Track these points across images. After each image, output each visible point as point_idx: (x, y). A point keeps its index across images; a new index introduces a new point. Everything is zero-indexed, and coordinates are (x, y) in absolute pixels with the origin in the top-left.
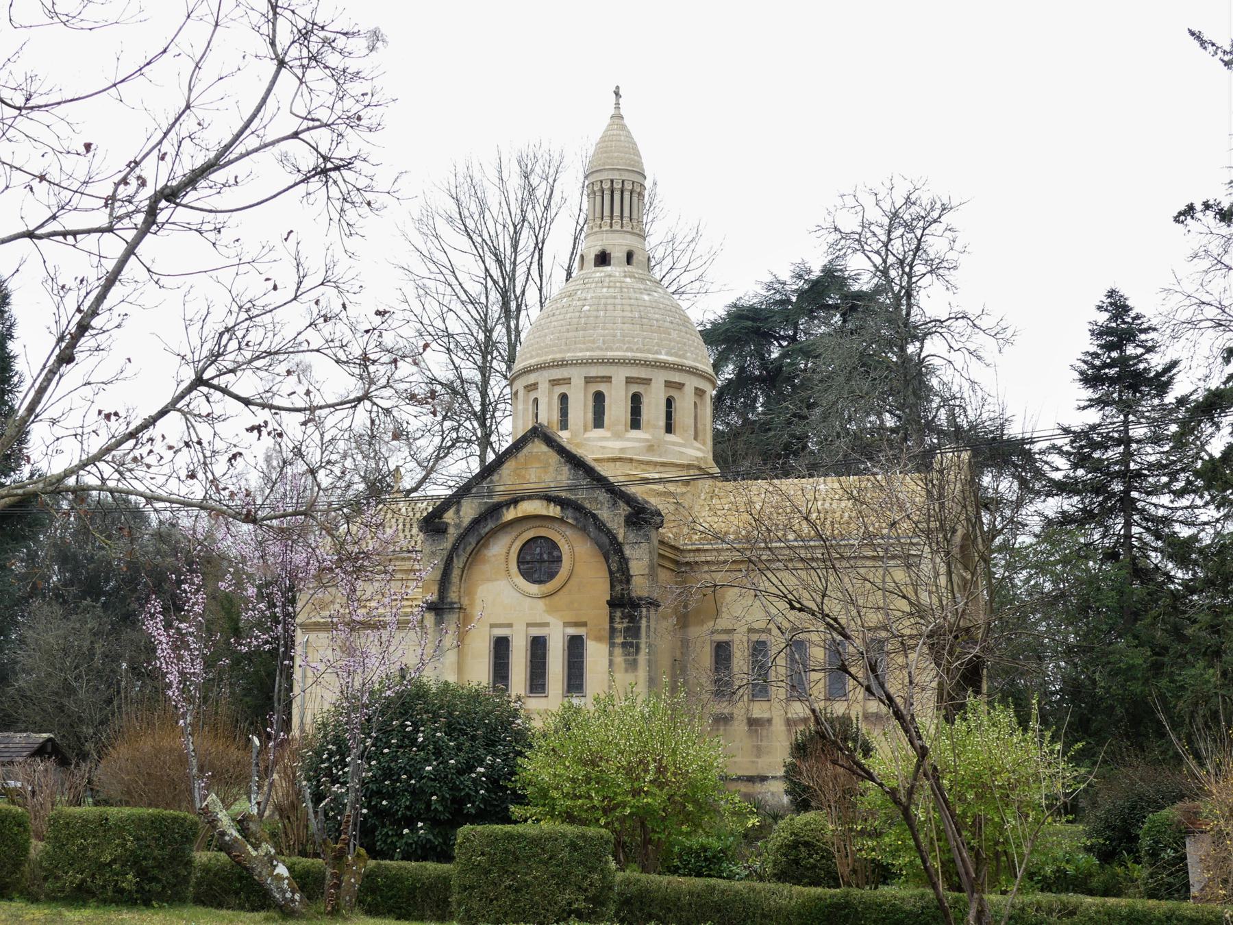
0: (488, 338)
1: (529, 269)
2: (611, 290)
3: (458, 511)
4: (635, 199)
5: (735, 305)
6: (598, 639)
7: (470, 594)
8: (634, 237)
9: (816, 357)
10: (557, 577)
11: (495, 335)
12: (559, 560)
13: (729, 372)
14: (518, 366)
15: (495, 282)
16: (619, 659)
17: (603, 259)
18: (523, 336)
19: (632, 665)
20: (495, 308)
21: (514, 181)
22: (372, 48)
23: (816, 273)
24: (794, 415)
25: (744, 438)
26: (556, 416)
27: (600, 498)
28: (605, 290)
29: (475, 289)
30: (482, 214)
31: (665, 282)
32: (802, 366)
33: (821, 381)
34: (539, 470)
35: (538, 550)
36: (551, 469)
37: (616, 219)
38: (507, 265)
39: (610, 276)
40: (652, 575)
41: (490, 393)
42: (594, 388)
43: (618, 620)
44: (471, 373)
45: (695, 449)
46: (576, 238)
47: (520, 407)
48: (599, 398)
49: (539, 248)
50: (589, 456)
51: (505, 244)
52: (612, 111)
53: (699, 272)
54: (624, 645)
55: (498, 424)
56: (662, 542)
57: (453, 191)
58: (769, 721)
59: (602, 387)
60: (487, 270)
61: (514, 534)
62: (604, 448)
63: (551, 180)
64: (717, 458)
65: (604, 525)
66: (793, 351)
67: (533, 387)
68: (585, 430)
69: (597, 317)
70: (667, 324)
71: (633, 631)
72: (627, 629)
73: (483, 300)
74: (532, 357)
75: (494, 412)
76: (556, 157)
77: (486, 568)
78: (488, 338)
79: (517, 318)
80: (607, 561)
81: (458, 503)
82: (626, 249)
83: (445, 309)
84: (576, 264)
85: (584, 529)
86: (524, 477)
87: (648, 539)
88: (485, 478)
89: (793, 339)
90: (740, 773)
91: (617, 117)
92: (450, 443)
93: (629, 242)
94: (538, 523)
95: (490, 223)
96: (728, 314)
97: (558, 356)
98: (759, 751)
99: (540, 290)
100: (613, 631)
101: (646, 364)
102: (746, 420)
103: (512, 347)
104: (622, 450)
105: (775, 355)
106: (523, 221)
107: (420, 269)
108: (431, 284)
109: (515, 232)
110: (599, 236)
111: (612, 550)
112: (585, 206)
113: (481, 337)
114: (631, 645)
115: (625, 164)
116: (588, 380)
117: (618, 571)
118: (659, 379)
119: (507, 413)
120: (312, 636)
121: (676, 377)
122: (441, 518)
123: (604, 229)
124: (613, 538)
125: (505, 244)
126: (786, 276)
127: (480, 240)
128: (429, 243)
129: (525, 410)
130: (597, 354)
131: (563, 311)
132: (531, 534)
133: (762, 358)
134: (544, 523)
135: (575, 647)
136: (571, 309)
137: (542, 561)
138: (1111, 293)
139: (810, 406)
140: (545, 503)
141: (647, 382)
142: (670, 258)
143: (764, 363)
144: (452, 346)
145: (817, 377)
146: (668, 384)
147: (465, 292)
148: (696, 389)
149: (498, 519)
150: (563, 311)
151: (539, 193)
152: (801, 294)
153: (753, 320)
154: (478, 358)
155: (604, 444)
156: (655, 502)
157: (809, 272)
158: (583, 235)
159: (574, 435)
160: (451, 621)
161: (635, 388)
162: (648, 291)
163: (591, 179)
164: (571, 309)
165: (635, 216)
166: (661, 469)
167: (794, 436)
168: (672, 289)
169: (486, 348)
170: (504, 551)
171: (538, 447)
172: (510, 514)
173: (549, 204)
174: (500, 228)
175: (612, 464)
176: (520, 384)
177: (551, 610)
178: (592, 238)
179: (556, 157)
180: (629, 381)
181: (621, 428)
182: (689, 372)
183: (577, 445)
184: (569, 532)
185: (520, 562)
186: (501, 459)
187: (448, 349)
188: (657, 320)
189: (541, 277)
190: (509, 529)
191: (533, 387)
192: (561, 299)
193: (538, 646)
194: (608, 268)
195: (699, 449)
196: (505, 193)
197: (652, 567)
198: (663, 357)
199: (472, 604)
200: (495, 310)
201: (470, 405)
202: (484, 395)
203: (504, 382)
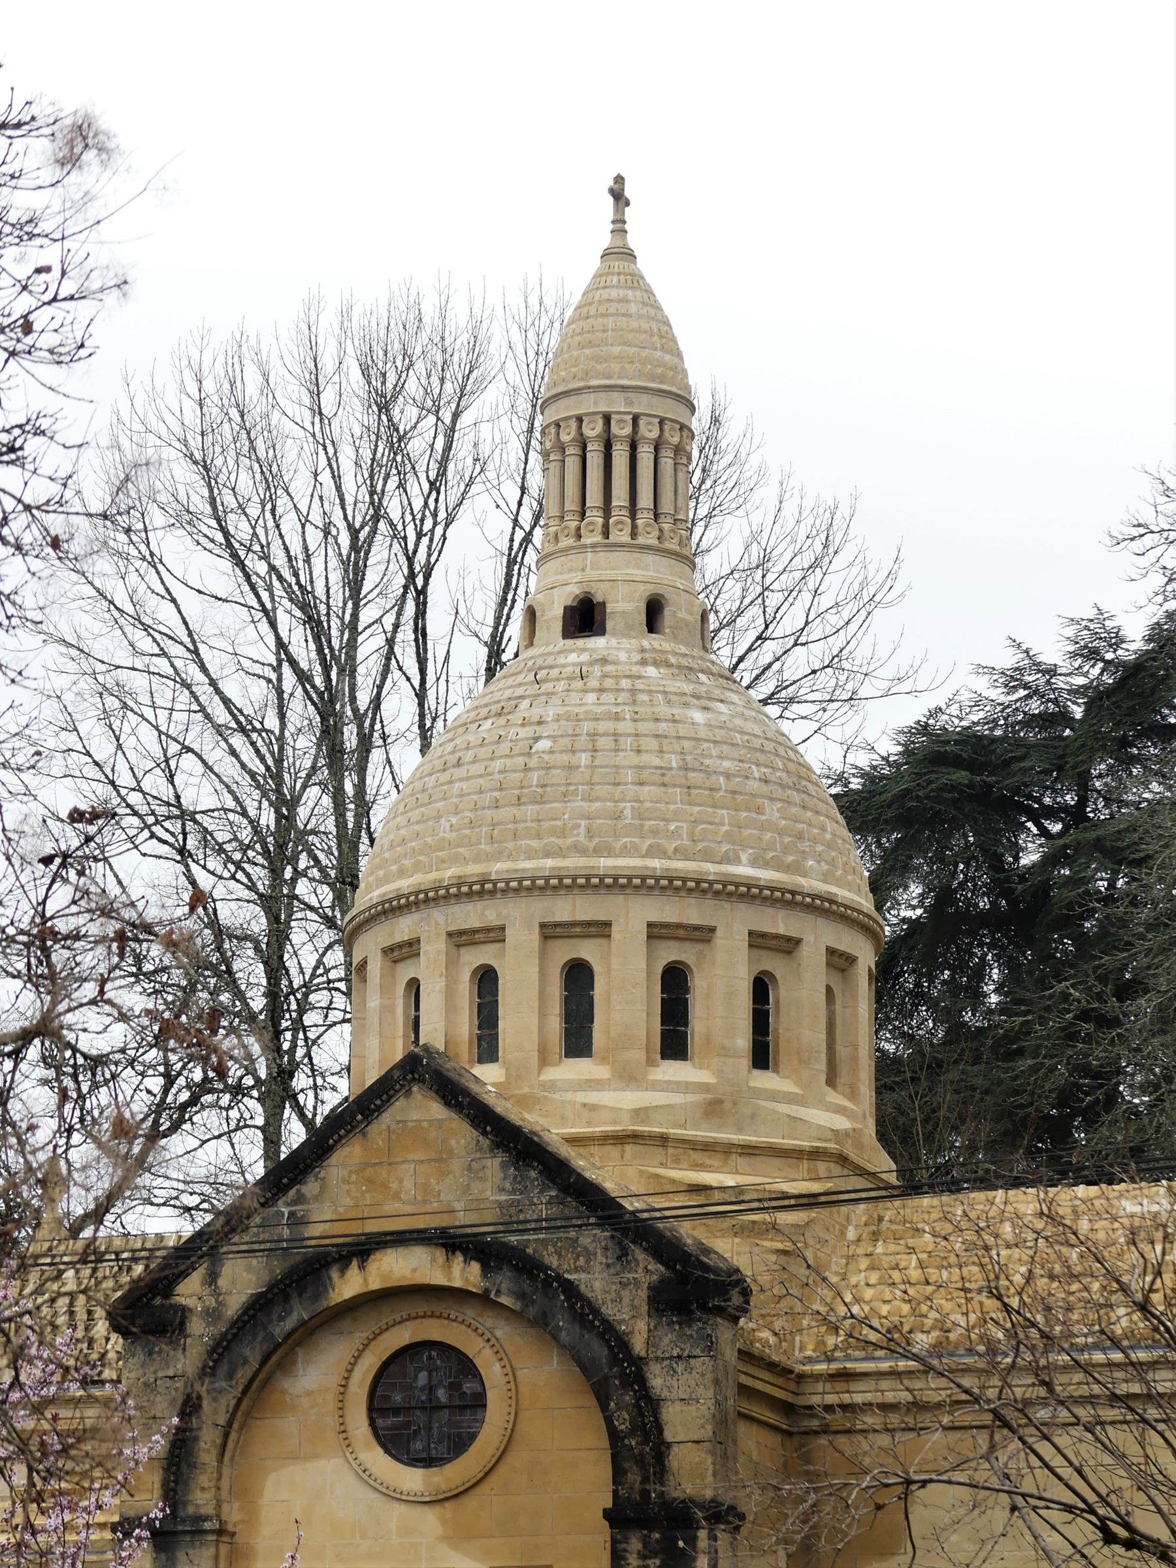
0: (286, 820)
1: (390, 642)
2: (608, 698)
3: (212, 1278)
4: (667, 463)
5: (924, 729)
7: (247, 1493)
8: (666, 561)
9: (1138, 863)
10: (474, 1449)
11: (302, 812)
12: (478, 1402)
13: (910, 903)
14: (367, 896)
15: (303, 677)
17: (585, 618)
18: (377, 816)
20: (303, 742)
21: (352, 419)
22: (69, 161)
23: (1135, 636)
24: (1084, 1016)
25: (953, 1075)
26: (466, 1025)
28: (591, 698)
29: (250, 694)
30: (269, 503)
31: (745, 675)
32: (1102, 885)
33: (1150, 927)
34: (429, 1175)
36: (456, 1165)
37: (619, 514)
38: (335, 633)
39: (604, 661)
40: (722, 1444)
41: (291, 964)
42: (565, 952)
44: (239, 911)
45: (827, 1110)
46: (511, 562)
47: (374, 1002)
48: (578, 977)
49: (416, 587)
50: (553, 1127)
51: (325, 575)
52: (605, 240)
53: (836, 643)
55: (310, 1044)
56: (746, 1355)
57: (195, 442)
59: (587, 950)
60: (281, 645)
61: (359, 1337)
62: (593, 1108)
63: (447, 416)
64: (891, 1131)
65: (596, 1312)
66: (1078, 846)
67: (406, 951)
68: (544, 1061)
69: (570, 768)
70: (753, 785)
73: (272, 722)
74: (402, 873)
75: (301, 1011)
76: (460, 357)
78: (286, 820)
79: (362, 771)
80: (604, 1407)
82: (643, 592)
83: (174, 748)
84: (515, 629)
85: (542, 1323)
86: (385, 1186)
87: (710, 1347)
88: (284, 1190)
89: (1076, 816)
91: (619, 253)
92: (185, 1096)
93: (653, 573)
94: (422, 1307)
95: (289, 524)
96: (907, 752)
97: (473, 870)
99: (421, 695)
101: (700, 888)
102: (957, 1030)
103: (348, 844)
104: (639, 1113)
105: (1030, 858)
106: (376, 518)
107: (109, 645)
108: (138, 683)
109: (354, 546)
110: (575, 559)
111: (616, 1381)
112: (535, 480)
113: (268, 818)
115: (640, 374)
116: (550, 932)
117: (632, 1432)
118: (734, 926)
119: (335, 1016)
121: (780, 923)
122: (168, 1292)
123: (587, 540)
124: (618, 1344)
125: (325, 575)
126: (1053, 652)
127: (262, 568)
128: (133, 578)
129: (387, 1010)
130: (573, 863)
131: (484, 752)
132: (402, 1336)
133: (996, 864)
134: (438, 1308)
136: (504, 748)
137: (432, 1407)
139: (1127, 991)
140: (440, 1254)
141: (702, 934)
142: (756, 610)
143: (1003, 878)
144: (191, 843)
145: (1145, 914)
146: (758, 940)
147: (227, 702)
148: (831, 952)
149: (317, 1297)
150: (484, 752)
151: (416, 446)
152: (1096, 698)
153: (972, 766)
154: (260, 874)
155: (593, 1097)
156: (729, 1249)
157: (1117, 641)
158: (531, 557)
159: (515, 1075)
161: (671, 953)
162: (704, 701)
163: (556, 412)
164: (504, 748)
165: (666, 506)
166: (742, 1162)
167: (1086, 1071)
168: (765, 688)
169: (281, 846)
170: (334, 1380)
171: (421, 1109)
172: (348, 1285)
173: (442, 471)
174: (314, 537)
175: (614, 1151)
176: (370, 946)
178: (553, 564)
179: (460, 357)
180: (657, 932)
181: (639, 1055)
182: (811, 908)
183: (525, 1102)
184: (503, 1331)
185: (376, 1408)
186: (326, 1138)
187: (182, 851)
188: (727, 775)
189: (423, 671)
190: (346, 1324)
191: (406, 951)
192: (478, 721)
194: (597, 643)
195: (840, 1110)
196: (326, 445)
197: (723, 1423)
198: (743, 870)
199: (251, 1520)
200: (304, 747)
201: (239, 995)
202: (275, 969)
203: (328, 936)
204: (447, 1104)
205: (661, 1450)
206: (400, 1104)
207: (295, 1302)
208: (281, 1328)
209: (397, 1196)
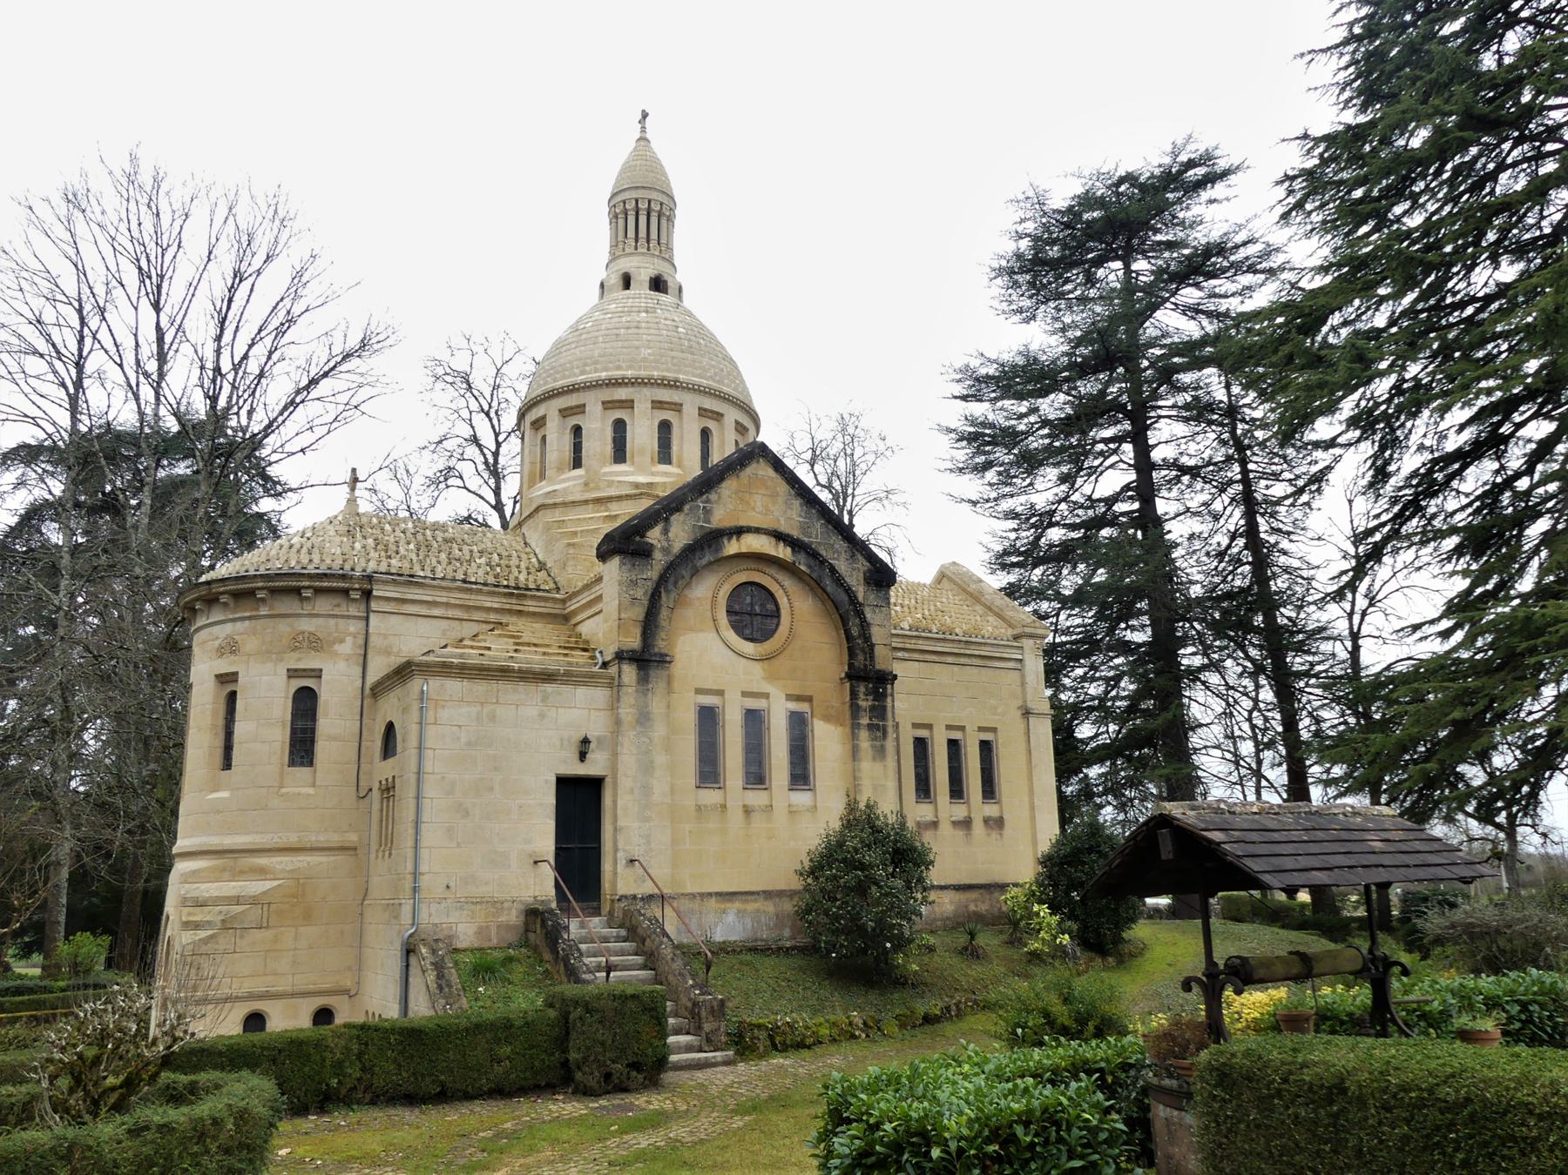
3: (666, 531)
4: (664, 222)
6: (827, 718)
35: (748, 600)
36: (780, 500)
37: (642, 241)
43: (862, 696)
52: (638, 135)
54: (870, 727)
59: (711, 425)
71: (879, 711)
72: (873, 708)
81: (667, 520)
88: (702, 494)
91: (643, 139)
100: (855, 710)
114: (877, 727)
121: (622, 394)
122: (643, 536)
123: (628, 250)
135: (799, 729)
140: (773, 540)
146: (703, 412)
165: (663, 241)
177: (771, 677)
185: (730, 612)
190: (715, 567)
193: (754, 720)
205: (872, 647)
206: (754, 465)
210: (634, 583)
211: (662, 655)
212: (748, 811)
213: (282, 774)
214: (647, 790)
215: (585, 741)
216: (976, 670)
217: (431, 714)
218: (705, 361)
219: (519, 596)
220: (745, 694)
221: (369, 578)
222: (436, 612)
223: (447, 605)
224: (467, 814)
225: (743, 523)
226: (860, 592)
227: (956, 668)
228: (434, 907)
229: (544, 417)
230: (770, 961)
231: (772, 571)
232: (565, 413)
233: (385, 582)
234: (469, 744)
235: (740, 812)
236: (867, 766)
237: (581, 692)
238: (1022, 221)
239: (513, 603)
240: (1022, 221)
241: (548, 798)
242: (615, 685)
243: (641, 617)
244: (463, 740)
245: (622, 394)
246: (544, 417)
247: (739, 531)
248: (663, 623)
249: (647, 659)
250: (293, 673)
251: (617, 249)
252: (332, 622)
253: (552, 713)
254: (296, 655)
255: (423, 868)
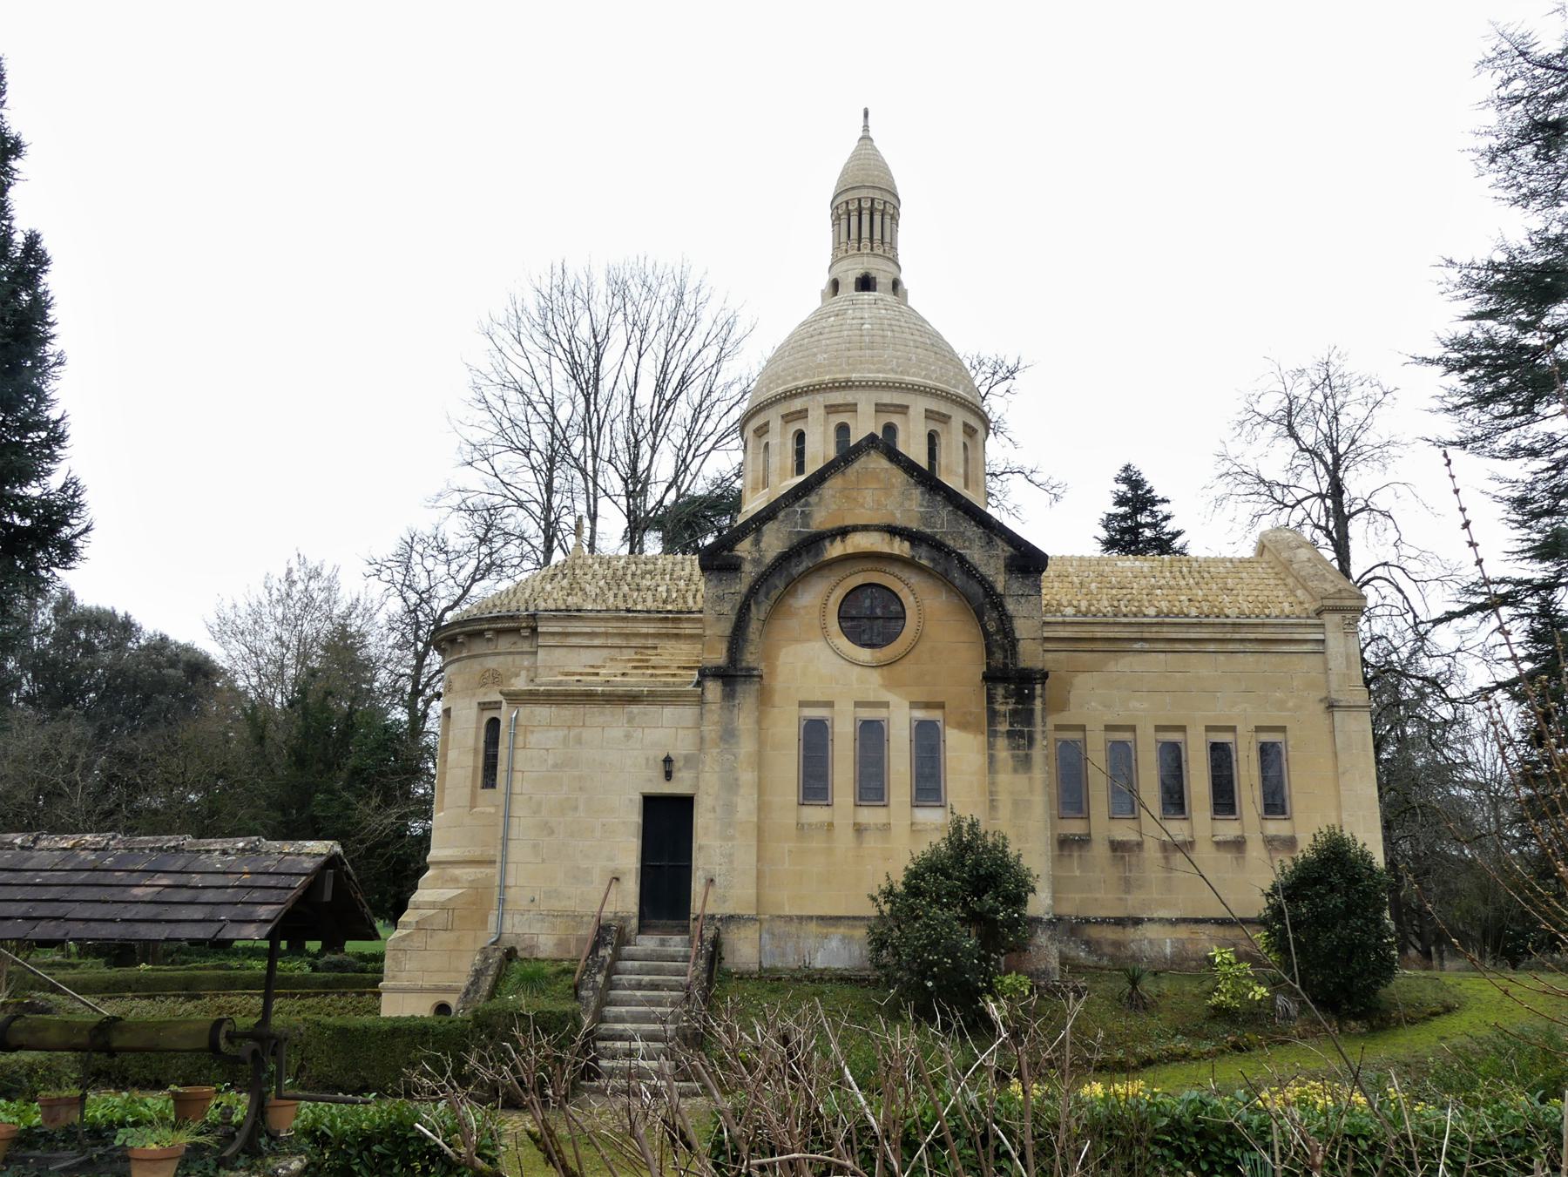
3: (757, 542)
6: (963, 726)
7: (769, 656)
12: (901, 616)
16: (1003, 752)
19: (1024, 763)
27: (969, 534)
35: (868, 603)
36: (895, 492)
37: (865, 241)
43: (1000, 699)
52: (861, 134)
54: (1010, 734)
58: (1140, 845)
59: (895, 419)
61: (833, 580)
71: (1023, 715)
72: (1014, 713)
77: (793, 623)
81: (758, 530)
88: (798, 498)
90: (1103, 913)
91: (866, 138)
97: (841, 376)
98: (1127, 885)
100: (992, 715)
114: (1021, 734)
117: (998, 632)
118: (866, 402)
120: (525, 711)
121: (797, 404)
122: (731, 550)
134: (880, 566)
135: (927, 742)
137: (873, 618)
138: (1127, 468)
140: (887, 536)
146: (930, 415)
160: (747, 696)
165: (887, 239)
170: (818, 602)
171: (876, 462)
172: (835, 550)
177: (889, 685)
185: (842, 617)
186: (820, 478)
190: (826, 572)
193: (872, 734)
204: (891, 460)
205: (1014, 642)
207: (804, 556)
208: (797, 570)
209: (862, 506)
210: (720, 599)
211: (750, 669)
212: (859, 829)
213: (474, 796)
214: (730, 808)
215: (668, 761)
216: (1251, 658)
217: (520, 739)
218: (886, 354)
219: (674, 620)
220: (858, 704)
221: (534, 616)
222: (597, 642)
223: (607, 635)
224: (552, 832)
225: (849, 521)
226: (1000, 582)
227: (1222, 657)
228: (517, 918)
229: (767, 424)
230: (848, 991)
231: (896, 570)
232: (788, 418)
233: (548, 619)
234: (555, 766)
235: (850, 832)
236: (1005, 778)
237: (668, 711)
238: (1506, 82)
239: (669, 628)
240: (1506, 82)
241: (635, 817)
242: (701, 701)
243: (728, 632)
244: (550, 762)
245: (797, 404)
246: (767, 424)
247: (843, 532)
248: (752, 636)
249: (732, 675)
250: (484, 706)
251: (839, 254)
252: (510, 658)
253: (638, 734)
254: (483, 690)
255: (510, 881)
